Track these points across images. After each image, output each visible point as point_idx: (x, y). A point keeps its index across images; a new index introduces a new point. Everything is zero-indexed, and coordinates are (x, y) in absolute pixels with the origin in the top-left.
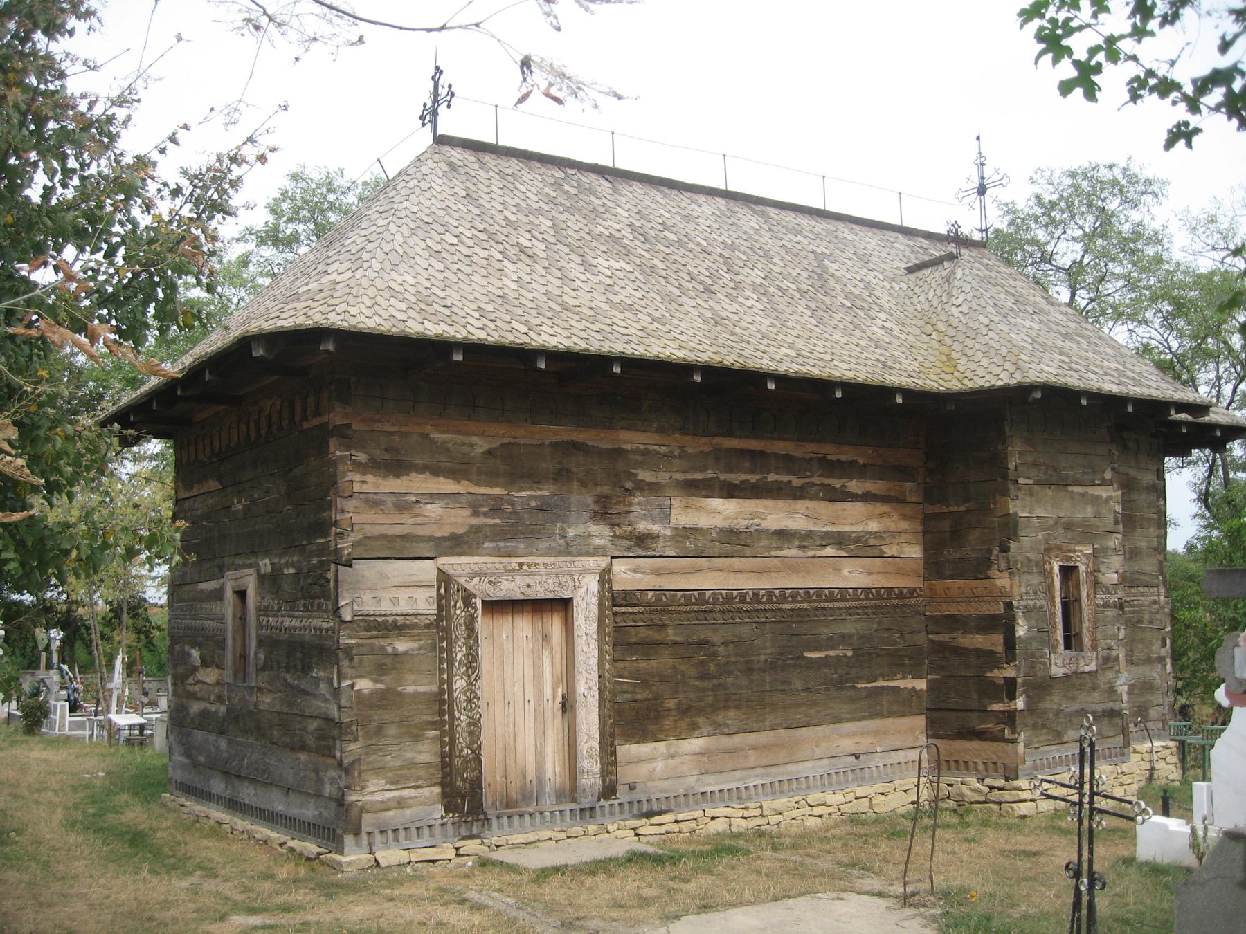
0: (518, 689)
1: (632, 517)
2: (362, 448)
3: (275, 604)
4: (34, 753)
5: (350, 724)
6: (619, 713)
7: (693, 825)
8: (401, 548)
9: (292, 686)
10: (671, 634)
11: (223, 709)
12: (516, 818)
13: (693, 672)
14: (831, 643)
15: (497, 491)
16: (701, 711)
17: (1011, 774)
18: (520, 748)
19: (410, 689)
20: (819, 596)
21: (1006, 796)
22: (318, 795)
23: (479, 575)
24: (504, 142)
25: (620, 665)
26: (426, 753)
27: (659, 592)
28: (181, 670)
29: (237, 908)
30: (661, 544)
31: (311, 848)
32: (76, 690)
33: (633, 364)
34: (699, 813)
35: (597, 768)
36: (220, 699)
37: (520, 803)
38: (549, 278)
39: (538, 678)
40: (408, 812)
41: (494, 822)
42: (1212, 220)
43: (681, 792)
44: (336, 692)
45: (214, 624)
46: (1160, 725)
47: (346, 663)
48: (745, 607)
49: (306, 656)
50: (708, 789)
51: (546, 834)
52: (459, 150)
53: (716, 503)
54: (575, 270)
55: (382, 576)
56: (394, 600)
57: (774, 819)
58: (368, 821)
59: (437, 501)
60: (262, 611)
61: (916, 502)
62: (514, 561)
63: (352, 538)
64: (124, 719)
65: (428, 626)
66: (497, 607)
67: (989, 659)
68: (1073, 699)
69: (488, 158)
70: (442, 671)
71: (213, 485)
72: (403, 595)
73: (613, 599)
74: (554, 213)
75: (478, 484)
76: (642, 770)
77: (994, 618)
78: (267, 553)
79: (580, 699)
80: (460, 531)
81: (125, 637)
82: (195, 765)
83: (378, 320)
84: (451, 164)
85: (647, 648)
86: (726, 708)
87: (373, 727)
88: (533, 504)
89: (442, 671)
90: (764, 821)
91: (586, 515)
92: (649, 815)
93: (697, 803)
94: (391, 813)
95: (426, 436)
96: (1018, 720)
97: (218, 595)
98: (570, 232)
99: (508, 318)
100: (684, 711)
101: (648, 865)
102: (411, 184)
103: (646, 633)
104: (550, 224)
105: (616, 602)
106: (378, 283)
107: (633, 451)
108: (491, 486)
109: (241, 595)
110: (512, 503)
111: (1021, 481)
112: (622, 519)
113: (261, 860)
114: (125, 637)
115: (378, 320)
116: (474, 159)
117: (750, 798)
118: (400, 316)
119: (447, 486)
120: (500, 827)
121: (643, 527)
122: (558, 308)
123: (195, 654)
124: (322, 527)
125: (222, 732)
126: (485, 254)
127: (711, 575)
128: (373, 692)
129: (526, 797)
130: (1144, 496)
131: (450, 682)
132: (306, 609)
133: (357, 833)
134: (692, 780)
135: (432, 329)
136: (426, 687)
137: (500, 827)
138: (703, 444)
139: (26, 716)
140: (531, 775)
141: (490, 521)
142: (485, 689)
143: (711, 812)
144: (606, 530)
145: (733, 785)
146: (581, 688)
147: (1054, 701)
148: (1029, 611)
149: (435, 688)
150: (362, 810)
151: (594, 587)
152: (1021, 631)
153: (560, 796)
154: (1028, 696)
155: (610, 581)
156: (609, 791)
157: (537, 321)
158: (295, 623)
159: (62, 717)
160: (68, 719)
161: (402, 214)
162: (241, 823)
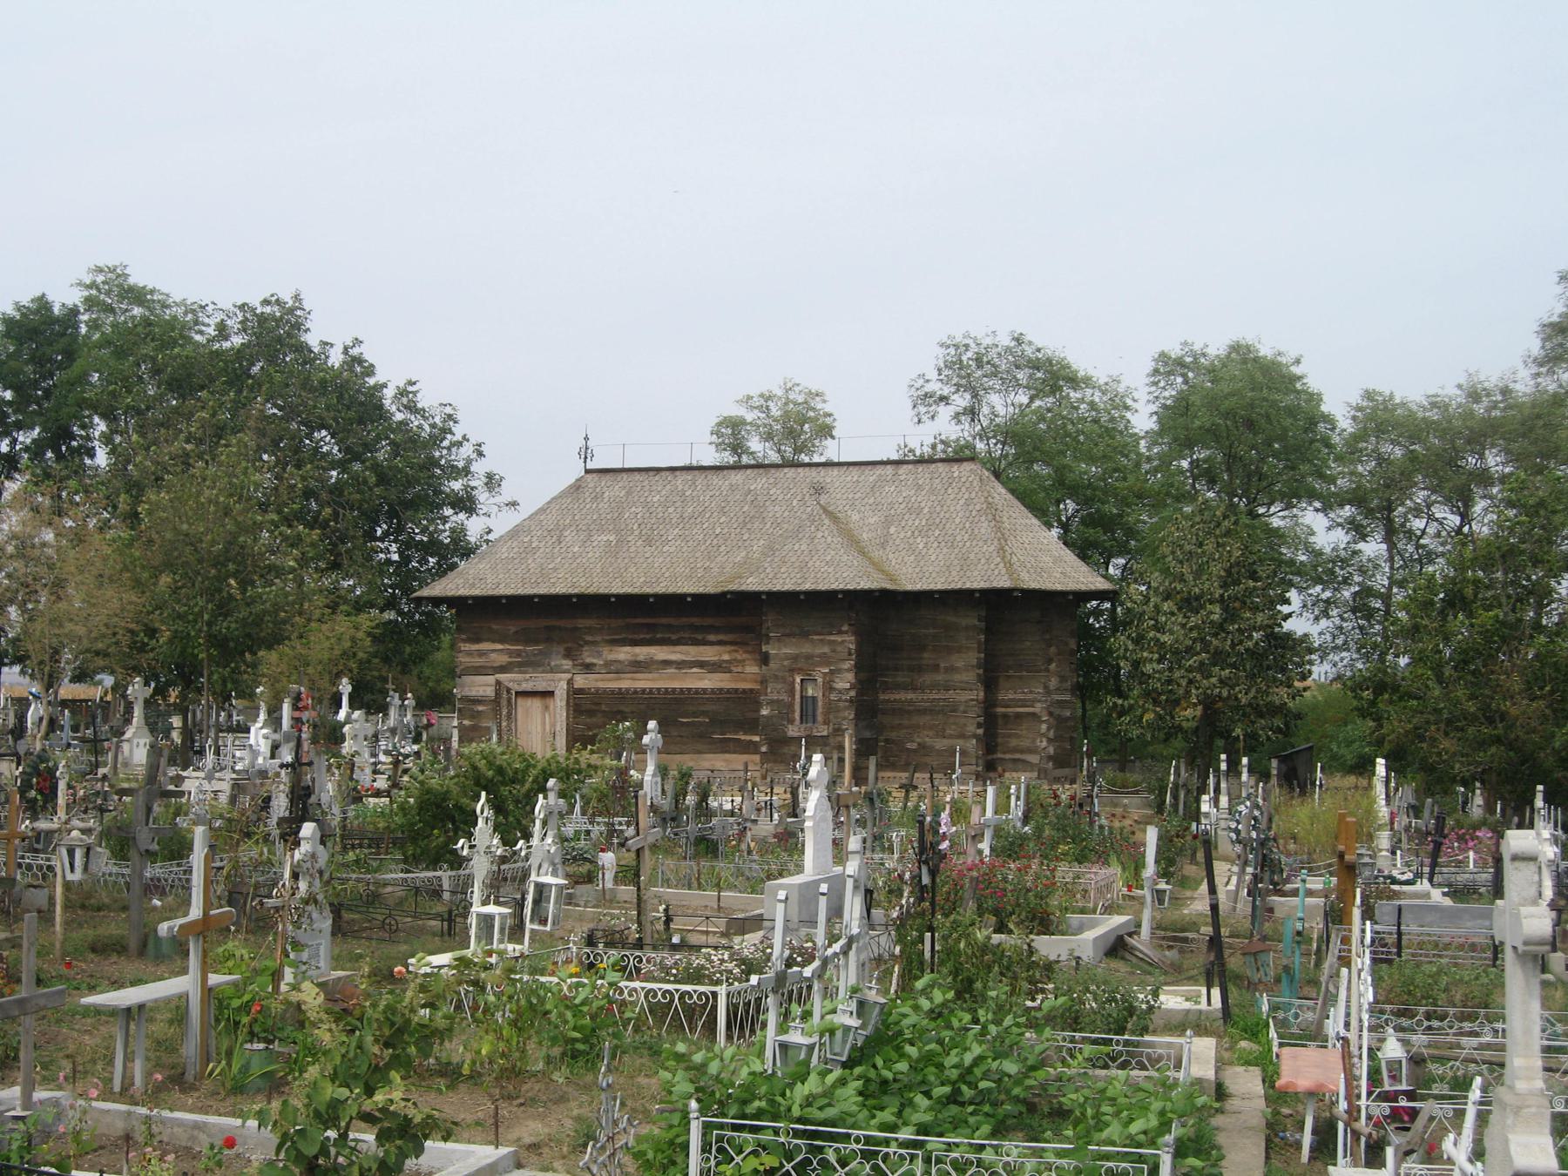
14: (694, 715)
27: (597, 690)
33: (580, 596)
39: (544, 723)
59: (496, 652)
61: (1179, 631)
85: (591, 713)
105: (574, 694)
121: (588, 660)
138: (620, 622)
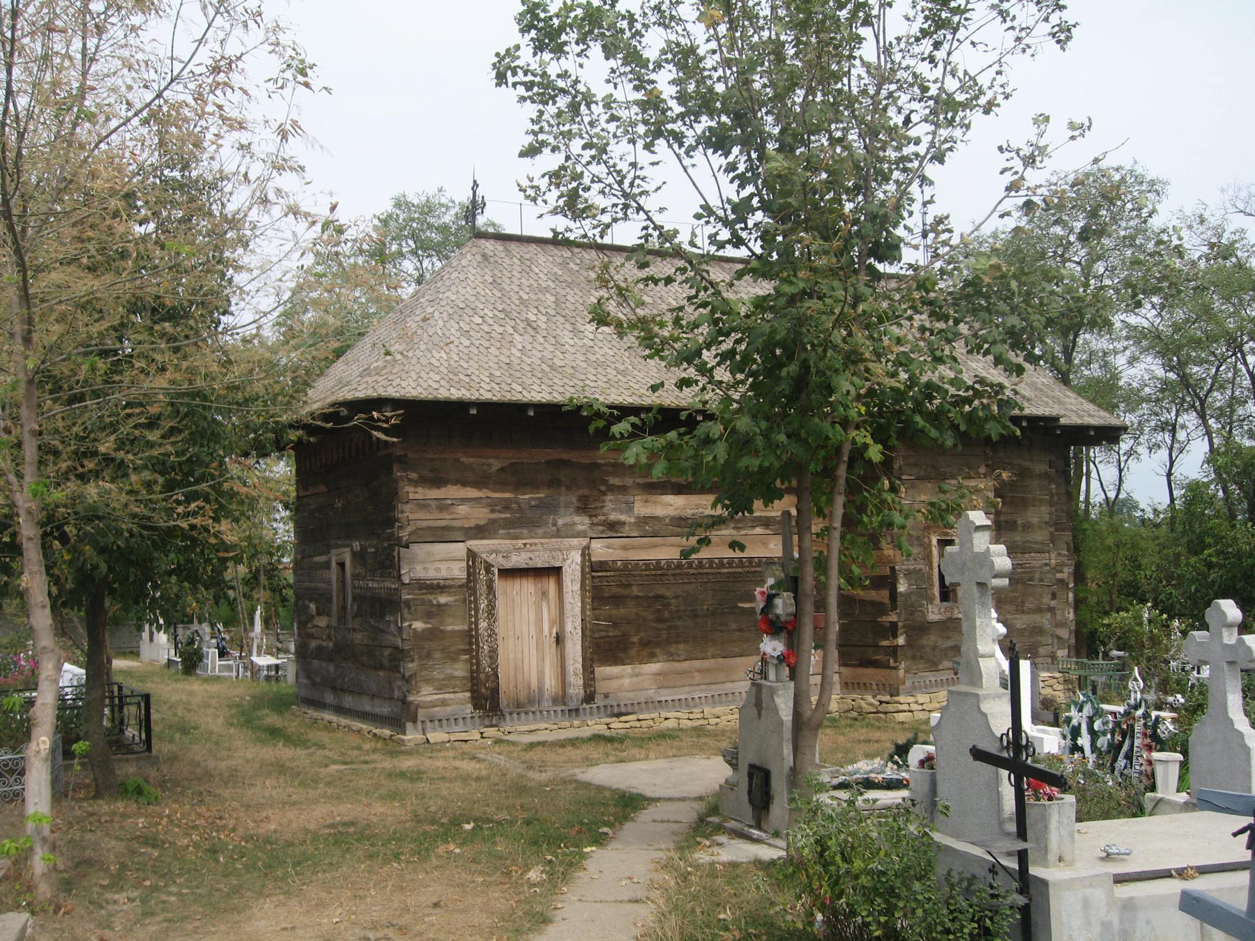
0: (525, 629)
1: (605, 510)
2: (414, 470)
3: (363, 572)
4: (194, 686)
5: (409, 651)
6: (597, 645)
7: (651, 723)
8: (442, 535)
9: (374, 627)
10: (635, 591)
11: (331, 644)
12: (523, 715)
13: (651, 617)
15: (507, 495)
16: (657, 644)
17: (894, 692)
18: (526, 668)
19: (449, 628)
20: (751, 563)
21: (890, 708)
22: (391, 698)
23: (497, 552)
24: (526, 233)
25: (597, 612)
26: (460, 670)
27: (626, 562)
28: (303, 618)
29: (335, 762)
30: (627, 528)
31: (387, 732)
32: (223, 639)
33: (487, 407)
34: (655, 715)
35: (581, 682)
36: (329, 637)
37: (526, 705)
38: (547, 345)
39: (539, 621)
40: (449, 709)
41: (508, 716)
42: (1202, 221)
43: (643, 700)
44: (400, 629)
45: (324, 586)
46: (1050, 660)
47: (406, 611)
48: (692, 571)
49: (382, 607)
50: (663, 699)
51: (543, 725)
52: (492, 242)
53: (669, 498)
54: (566, 337)
55: (429, 554)
56: (438, 570)
57: (713, 721)
58: (422, 714)
59: (466, 503)
60: (355, 576)
62: (520, 542)
63: (409, 529)
64: (264, 661)
65: (461, 586)
66: (508, 573)
67: (880, 608)
68: (948, 638)
69: (513, 246)
70: (470, 616)
71: (323, 488)
72: (443, 566)
73: (592, 566)
74: (558, 290)
75: (494, 491)
76: (614, 684)
77: (884, 578)
78: (357, 538)
79: (568, 635)
80: (482, 523)
81: (262, 595)
82: (314, 684)
83: (420, 389)
84: (485, 256)
85: (617, 600)
86: (677, 642)
87: (425, 652)
88: (533, 503)
89: (470, 616)
90: (705, 722)
91: (572, 510)
92: (618, 715)
93: (655, 708)
94: (436, 709)
95: (458, 460)
96: (899, 653)
97: (327, 566)
98: (568, 305)
99: (509, 381)
100: (645, 644)
101: (603, 743)
102: (453, 277)
103: (615, 590)
104: (553, 299)
105: (594, 569)
106: (423, 361)
107: (606, 464)
108: (503, 492)
109: (342, 565)
110: (518, 504)
111: (904, 477)
112: (598, 511)
113: (354, 740)
114: (262, 595)
115: (420, 389)
116: (501, 248)
117: (695, 706)
118: (435, 385)
119: (473, 493)
120: (512, 720)
121: (613, 517)
122: (548, 369)
123: (313, 606)
124: (390, 522)
125: (331, 660)
126: (500, 330)
127: (665, 549)
128: (424, 630)
129: (531, 701)
130: (1036, 482)
131: (477, 624)
132: (382, 576)
133: (415, 721)
134: (651, 692)
135: (456, 394)
136: (460, 627)
137: (512, 720)
139: (184, 661)
140: (534, 685)
141: (503, 516)
142: (500, 629)
143: (664, 714)
144: (586, 520)
145: (682, 697)
146: (569, 627)
147: (931, 639)
148: (908, 574)
149: (466, 627)
150: (418, 706)
151: (578, 559)
152: (902, 587)
153: (555, 701)
154: (908, 636)
155: (589, 555)
156: (589, 698)
157: (530, 382)
158: (375, 585)
159: (213, 662)
160: (218, 663)
161: (443, 303)
162: (344, 721)
